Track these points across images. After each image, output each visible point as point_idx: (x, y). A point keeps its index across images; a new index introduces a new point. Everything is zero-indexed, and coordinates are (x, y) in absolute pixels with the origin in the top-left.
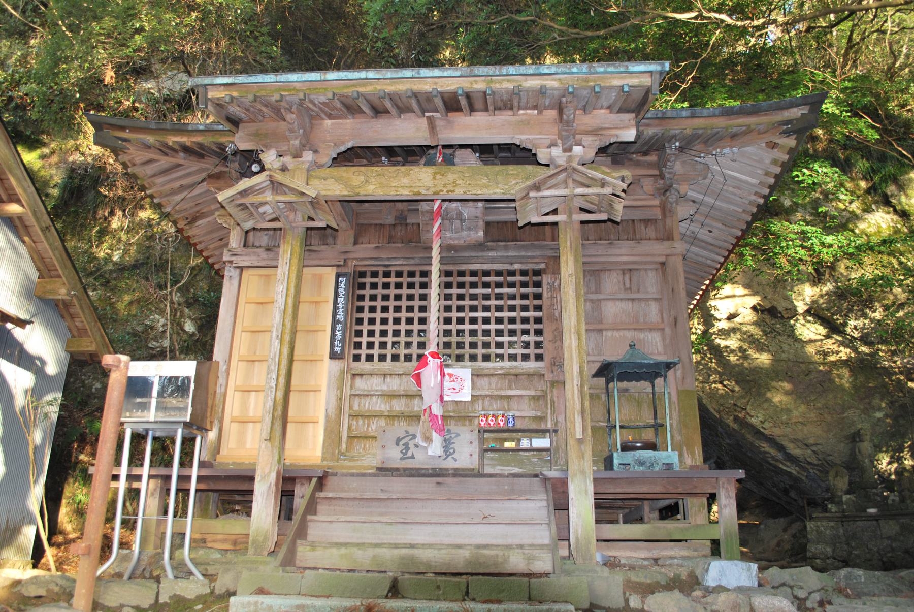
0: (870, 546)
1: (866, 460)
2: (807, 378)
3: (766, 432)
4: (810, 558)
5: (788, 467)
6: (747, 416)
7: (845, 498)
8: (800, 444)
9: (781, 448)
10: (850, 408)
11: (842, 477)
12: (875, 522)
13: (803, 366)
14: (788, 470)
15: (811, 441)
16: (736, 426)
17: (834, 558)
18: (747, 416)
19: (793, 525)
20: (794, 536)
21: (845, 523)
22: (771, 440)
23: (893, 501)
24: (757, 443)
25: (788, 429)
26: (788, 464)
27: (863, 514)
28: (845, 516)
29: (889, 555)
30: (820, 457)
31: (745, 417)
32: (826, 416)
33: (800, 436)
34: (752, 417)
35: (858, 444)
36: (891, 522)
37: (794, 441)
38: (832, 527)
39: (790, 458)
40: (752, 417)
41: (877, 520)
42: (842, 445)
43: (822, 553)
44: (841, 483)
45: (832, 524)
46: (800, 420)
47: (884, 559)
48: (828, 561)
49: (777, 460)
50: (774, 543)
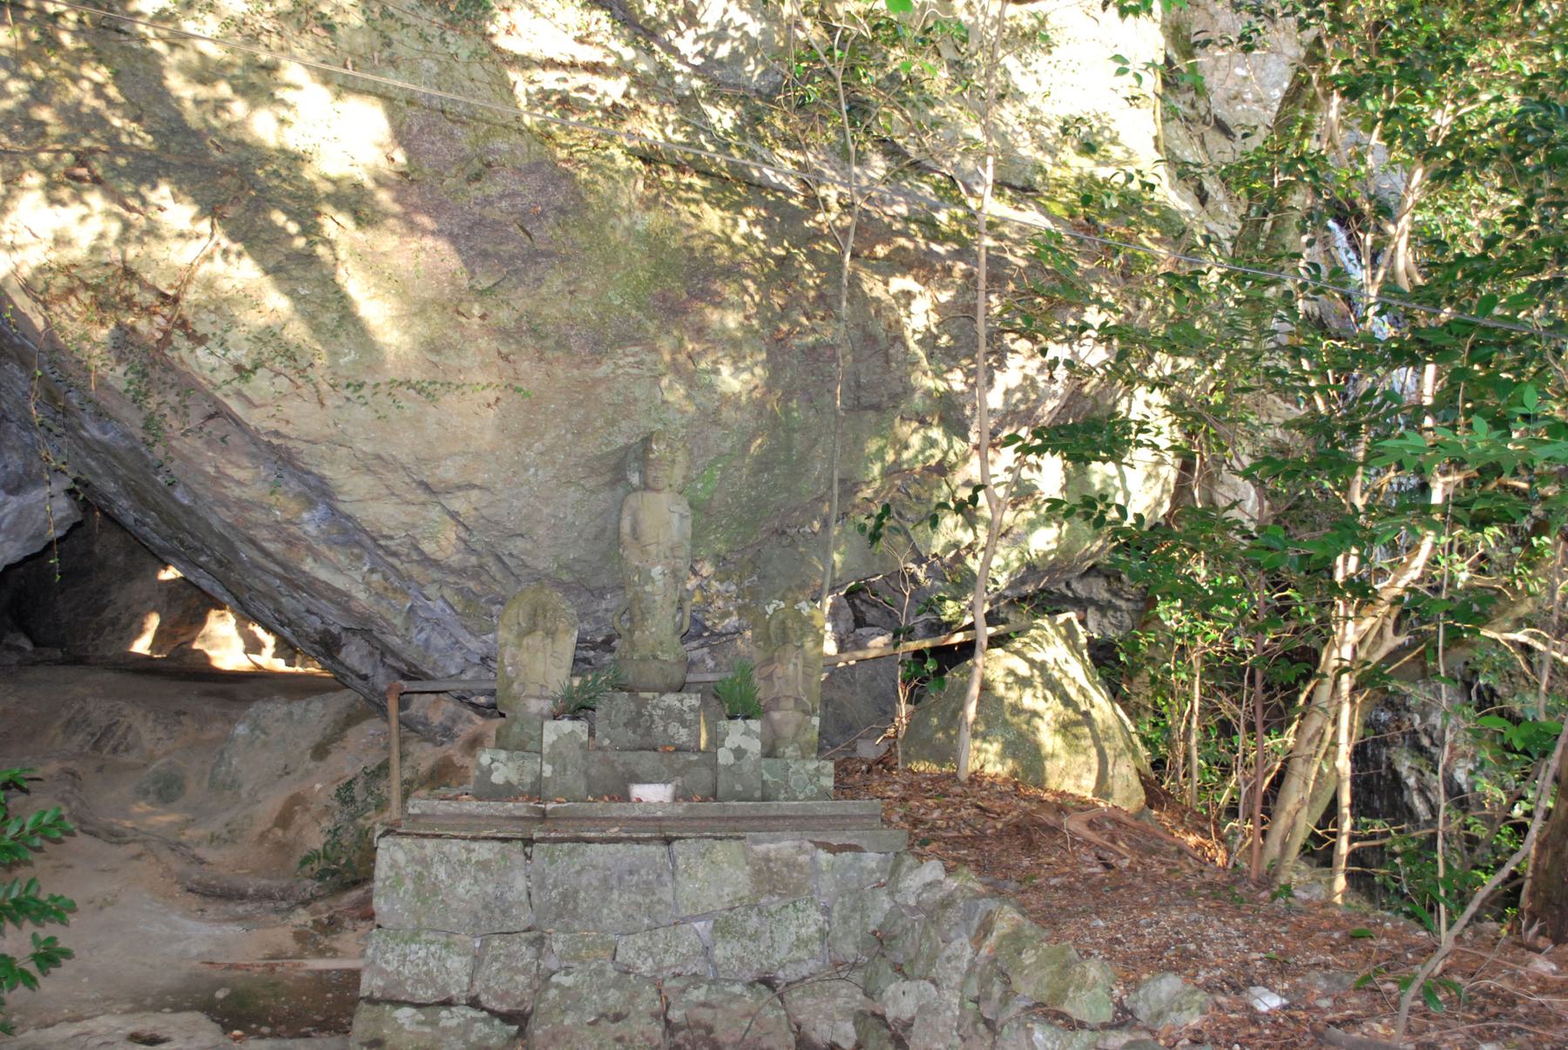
0: (626, 954)
1: (656, 571)
2: (474, 190)
3: (256, 419)
4: (371, 1001)
5: (339, 570)
6: (178, 337)
7: (552, 732)
8: (397, 480)
9: (319, 492)
10: (623, 339)
11: (551, 634)
12: (656, 850)
13: (465, 139)
14: (340, 582)
15: (449, 471)
16: (118, 375)
17: (474, 1003)
18: (178, 337)
19: (352, 733)
20: (345, 794)
21: (537, 851)
22: (281, 458)
23: (739, 753)
24: (209, 461)
25: (360, 413)
26: (342, 559)
27: (616, 809)
28: (543, 816)
29: (698, 994)
30: (477, 541)
31: (166, 340)
32: (525, 366)
33: (403, 446)
34: (201, 340)
35: (633, 500)
36: (721, 851)
37: (375, 464)
38: (484, 865)
39: (350, 535)
40: (201, 340)
41: (668, 841)
42: (573, 494)
43: (428, 979)
44: (543, 665)
45: (484, 851)
46: (415, 376)
47: (676, 1015)
48: (448, 1018)
49: (291, 542)
50: (272, 804)
